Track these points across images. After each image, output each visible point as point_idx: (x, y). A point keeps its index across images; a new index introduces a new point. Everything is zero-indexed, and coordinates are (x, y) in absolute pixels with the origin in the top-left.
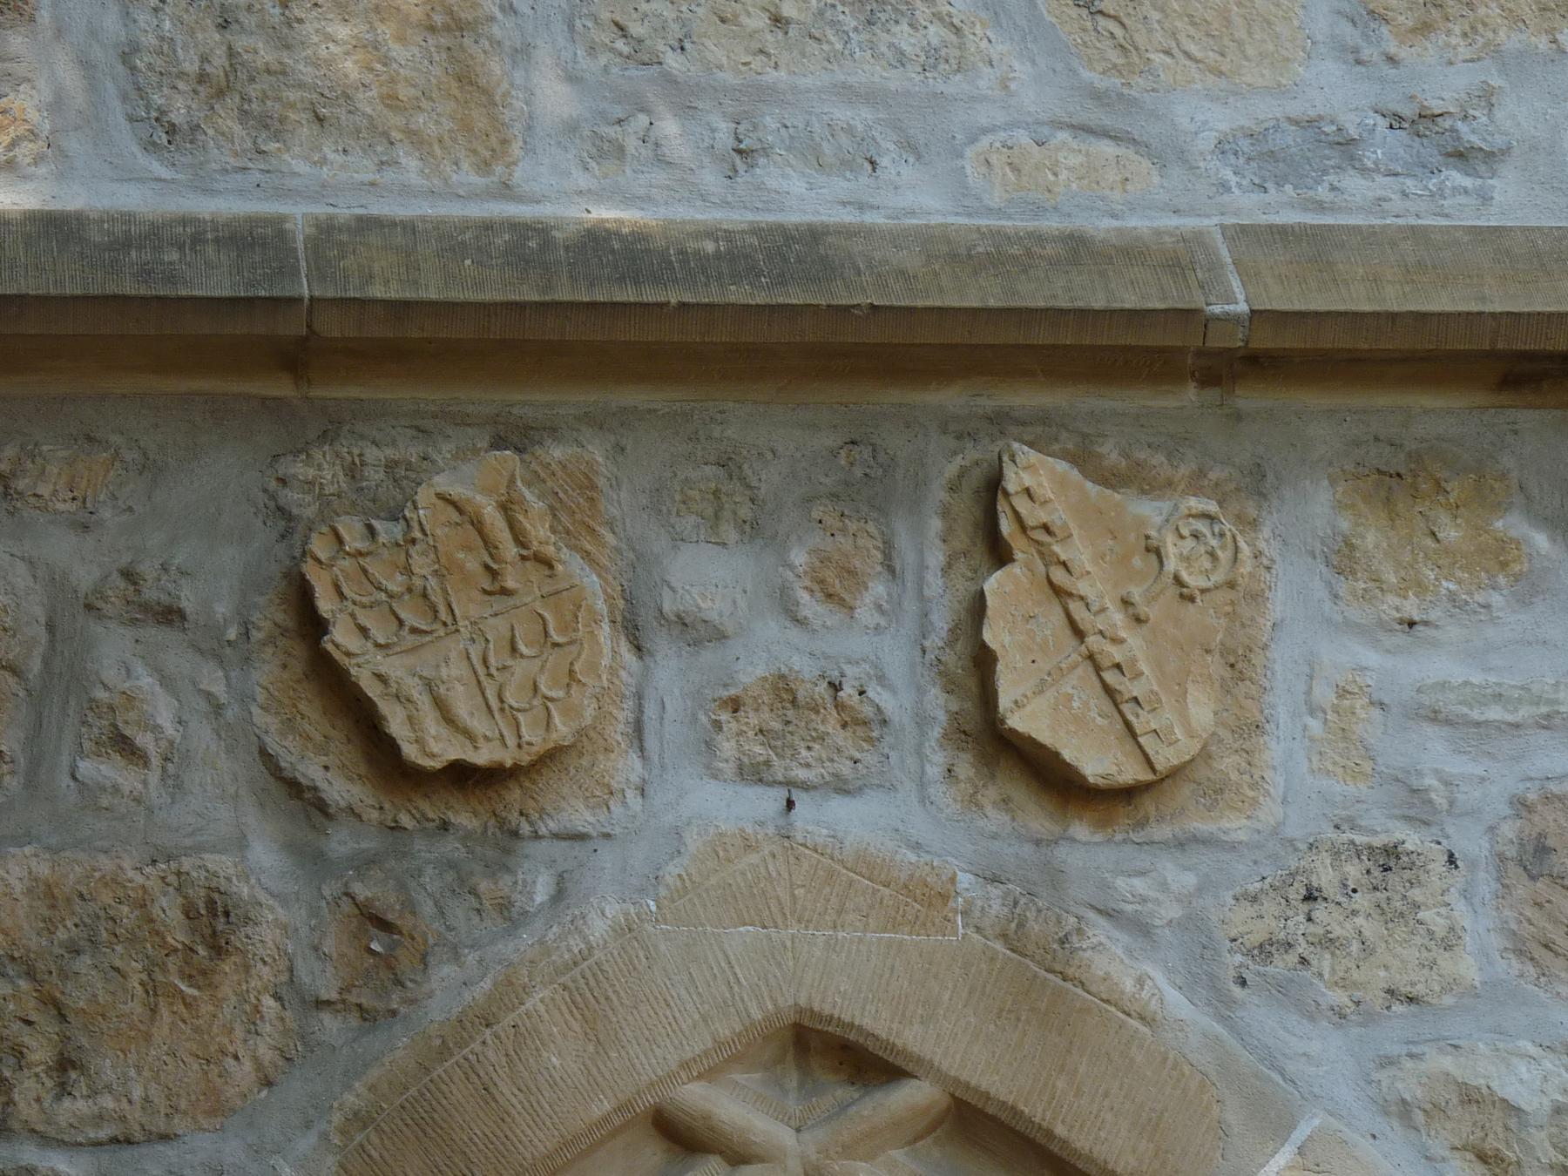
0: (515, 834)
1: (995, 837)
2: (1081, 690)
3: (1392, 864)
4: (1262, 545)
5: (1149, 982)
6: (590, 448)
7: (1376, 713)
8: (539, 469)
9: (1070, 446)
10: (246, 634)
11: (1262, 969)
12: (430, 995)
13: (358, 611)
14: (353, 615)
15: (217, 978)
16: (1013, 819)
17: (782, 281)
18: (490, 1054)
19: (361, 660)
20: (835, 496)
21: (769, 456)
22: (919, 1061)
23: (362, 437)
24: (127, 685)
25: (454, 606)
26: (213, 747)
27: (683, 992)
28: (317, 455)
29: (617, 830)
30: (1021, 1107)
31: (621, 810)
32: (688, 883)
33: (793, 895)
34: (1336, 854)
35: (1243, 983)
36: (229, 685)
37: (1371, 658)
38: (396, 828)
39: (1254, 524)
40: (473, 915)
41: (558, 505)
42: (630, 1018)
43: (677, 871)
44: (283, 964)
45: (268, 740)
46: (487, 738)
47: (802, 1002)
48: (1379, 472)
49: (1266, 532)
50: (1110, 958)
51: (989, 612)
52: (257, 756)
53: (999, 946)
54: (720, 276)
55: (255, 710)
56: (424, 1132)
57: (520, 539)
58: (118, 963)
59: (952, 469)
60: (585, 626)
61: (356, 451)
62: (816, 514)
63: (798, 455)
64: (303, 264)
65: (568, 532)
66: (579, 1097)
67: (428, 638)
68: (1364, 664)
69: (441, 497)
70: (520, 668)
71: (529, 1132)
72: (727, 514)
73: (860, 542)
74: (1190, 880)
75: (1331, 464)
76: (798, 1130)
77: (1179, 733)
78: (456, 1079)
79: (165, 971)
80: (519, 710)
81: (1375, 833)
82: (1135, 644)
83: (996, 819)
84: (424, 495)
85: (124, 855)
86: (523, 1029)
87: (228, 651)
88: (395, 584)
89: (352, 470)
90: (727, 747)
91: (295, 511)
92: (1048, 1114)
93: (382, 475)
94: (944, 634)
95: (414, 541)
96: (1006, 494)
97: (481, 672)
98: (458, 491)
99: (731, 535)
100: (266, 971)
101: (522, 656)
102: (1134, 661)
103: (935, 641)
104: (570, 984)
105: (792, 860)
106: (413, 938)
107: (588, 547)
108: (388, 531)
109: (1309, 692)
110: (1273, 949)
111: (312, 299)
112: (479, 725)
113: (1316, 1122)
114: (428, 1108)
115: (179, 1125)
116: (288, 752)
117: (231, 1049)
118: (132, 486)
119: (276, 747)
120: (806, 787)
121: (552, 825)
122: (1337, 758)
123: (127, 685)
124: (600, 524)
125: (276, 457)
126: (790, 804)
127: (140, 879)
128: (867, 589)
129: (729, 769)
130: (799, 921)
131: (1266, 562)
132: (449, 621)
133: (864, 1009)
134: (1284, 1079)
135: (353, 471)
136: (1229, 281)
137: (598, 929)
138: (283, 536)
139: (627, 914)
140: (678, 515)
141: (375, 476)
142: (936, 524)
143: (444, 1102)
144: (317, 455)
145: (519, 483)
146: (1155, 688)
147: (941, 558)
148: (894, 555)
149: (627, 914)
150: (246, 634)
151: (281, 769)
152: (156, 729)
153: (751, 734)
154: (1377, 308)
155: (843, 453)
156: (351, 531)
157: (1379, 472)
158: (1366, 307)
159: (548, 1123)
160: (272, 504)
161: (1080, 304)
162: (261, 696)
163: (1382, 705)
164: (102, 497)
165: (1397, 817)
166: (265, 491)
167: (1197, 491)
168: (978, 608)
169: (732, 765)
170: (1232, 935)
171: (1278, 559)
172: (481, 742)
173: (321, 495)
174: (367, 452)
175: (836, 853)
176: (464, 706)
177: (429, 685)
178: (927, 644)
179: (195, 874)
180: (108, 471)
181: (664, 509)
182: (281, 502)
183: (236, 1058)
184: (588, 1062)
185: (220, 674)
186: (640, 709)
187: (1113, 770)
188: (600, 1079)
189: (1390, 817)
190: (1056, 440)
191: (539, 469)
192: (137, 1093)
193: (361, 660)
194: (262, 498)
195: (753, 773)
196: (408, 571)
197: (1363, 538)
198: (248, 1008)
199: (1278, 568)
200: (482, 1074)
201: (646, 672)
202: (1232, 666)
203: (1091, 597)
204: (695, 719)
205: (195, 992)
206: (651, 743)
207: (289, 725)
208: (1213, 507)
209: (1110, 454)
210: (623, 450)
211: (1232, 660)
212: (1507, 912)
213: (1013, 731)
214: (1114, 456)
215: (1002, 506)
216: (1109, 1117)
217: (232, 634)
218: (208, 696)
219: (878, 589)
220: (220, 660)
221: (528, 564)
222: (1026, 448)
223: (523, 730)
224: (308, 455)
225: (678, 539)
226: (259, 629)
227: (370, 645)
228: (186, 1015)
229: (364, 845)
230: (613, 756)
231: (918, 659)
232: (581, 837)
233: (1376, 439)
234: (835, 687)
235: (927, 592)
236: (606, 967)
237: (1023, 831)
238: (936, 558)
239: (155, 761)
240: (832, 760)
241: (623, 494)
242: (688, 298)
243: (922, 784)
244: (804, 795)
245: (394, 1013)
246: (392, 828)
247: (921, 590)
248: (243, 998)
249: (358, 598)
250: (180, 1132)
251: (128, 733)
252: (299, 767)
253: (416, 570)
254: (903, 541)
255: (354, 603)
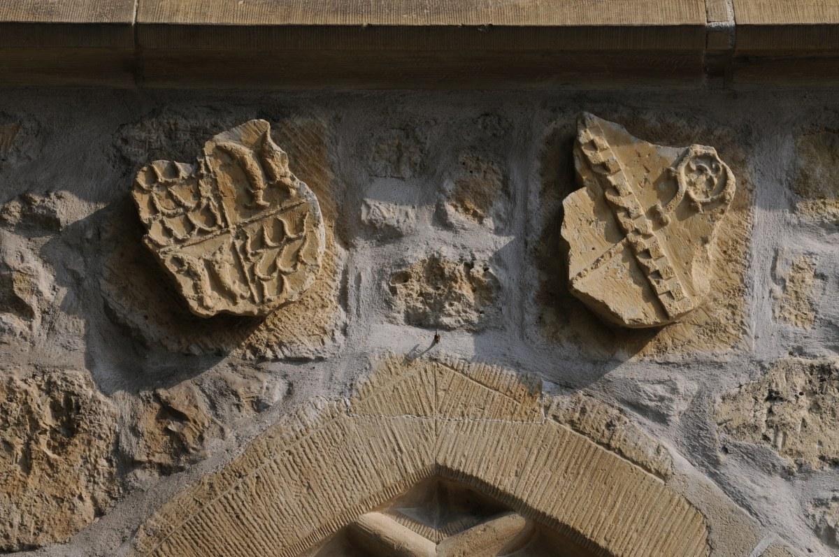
0: (263, 359)
1: (567, 359)
2: (617, 264)
3: (826, 377)
4: (747, 176)
5: (663, 450)
6: (320, 119)
7: (819, 282)
8: (286, 132)
9: (625, 115)
10: (99, 234)
11: (738, 442)
12: (204, 458)
13: (165, 219)
14: (162, 222)
15: (70, 448)
16: (580, 348)
17: (437, 11)
18: (241, 494)
19: (166, 249)
20: (473, 148)
21: (432, 123)
22: (514, 499)
23: (176, 113)
24: (22, 266)
25: (227, 215)
26: (75, 304)
27: (365, 456)
28: (148, 124)
29: (327, 356)
30: (578, 528)
31: (331, 343)
32: (371, 388)
33: (437, 395)
34: (789, 371)
35: (725, 450)
36: (86, 266)
37: (815, 245)
38: (189, 355)
39: (743, 163)
40: (234, 408)
41: (298, 155)
42: (330, 471)
43: (365, 380)
44: (112, 439)
45: (109, 300)
46: (242, 297)
47: (440, 462)
48: (827, 129)
49: (750, 168)
50: (641, 434)
51: (566, 218)
52: (102, 310)
53: (568, 428)
54: (399, 8)
55: (102, 281)
56: (197, 543)
57: (268, 173)
58: (8, 438)
59: (548, 131)
60: (307, 227)
61: (172, 121)
62: (461, 159)
63: (451, 122)
64: (718, 159)
65: (304, 171)
66: (296, 521)
67: (210, 236)
68: (811, 251)
69: (219, 148)
70: (266, 255)
71: (263, 543)
72: (404, 159)
73: (489, 176)
74: (694, 387)
75: (794, 125)
76: (438, 543)
77: (685, 293)
78: (218, 511)
79: (37, 442)
80: (264, 280)
81: (815, 357)
82: (659, 236)
83: (568, 348)
84: (209, 148)
85: (15, 371)
86: (262, 479)
87: (87, 245)
88: (190, 203)
89: (170, 134)
90: (400, 304)
91: (133, 159)
92: (595, 533)
93: (188, 137)
94: (539, 233)
95: (202, 176)
96: (579, 144)
97: (239, 256)
98: (231, 144)
99: (406, 171)
100: (102, 444)
101: (268, 247)
102: (657, 249)
103: (533, 237)
104: (294, 451)
105: (437, 374)
106: (195, 422)
107: (316, 180)
108: (184, 170)
109: (774, 268)
110: (746, 431)
111: (137, 23)
112: (237, 288)
113: (771, 540)
114: (200, 528)
115: (43, 540)
116: (122, 307)
117: (78, 492)
118: (29, 144)
119: (114, 304)
120: (448, 328)
121: (287, 353)
122: (792, 310)
123: (22, 266)
124: (324, 166)
125: (122, 126)
126: (437, 339)
127: (24, 386)
128: (491, 205)
129: (401, 317)
130: (440, 412)
131: (749, 187)
132: (223, 225)
133: (479, 466)
134: (751, 513)
135: (171, 134)
136: (725, 9)
137: (311, 416)
138: (124, 175)
139: (331, 407)
140: (374, 160)
141: (184, 137)
142: (537, 164)
143: (210, 524)
144: (148, 124)
145: (269, 139)
146: (671, 264)
147: (539, 186)
148: (510, 183)
149: (331, 407)
150: (99, 234)
151: (117, 318)
152: (39, 293)
153: (415, 296)
154: (819, 22)
155: (480, 121)
156: (160, 167)
157: (827, 129)
158: (812, 21)
159: (276, 537)
160: (118, 154)
161: (625, 23)
162: (106, 274)
163: (822, 277)
164: (10, 150)
165: (830, 348)
166: (114, 146)
167: (705, 141)
168: (557, 217)
169: (402, 315)
170: (719, 421)
171: (757, 184)
172: (240, 300)
173: (149, 149)
174: (179, 121)
175: (466, 369)
176: (229, 276)
177: (209, 265)
178: (529, 239)
179: (59, 383)
180: (15, 134)
181: (365, 156)
182: (124, 153)
183: (80, 498)
184: (303, 500)
185: (81, 259)
186: (345, 281)
187: (642, 316)
188: (309, 510)
189: (826, 347)
190: (616, 111)
191: (286, 132)
192: (17, 520)
193: (166, 249)
194: (112, 151)
195: (416, 320)
196: (197, 195)
197: (814, 171)
198: (89, 466)
199: (757, 191)
200: (235, 507)
201: (350, 259)
202: (725, 252)
203: (631, 208)
204: (379, 286)
205: (56, 456)
206: (352, 302)
207: (124, 290)
208: (712, 151)
209: (651, 120)
210: (340, 119)
211: (725, 249)
212: (306, 274)
213: (577, 291)
214: (653, 121)
215: (576, 152)
216: (635, 535)
217: (89, 235)
218: (74, 273)
219: (499, 205)
220: (81, 250)
221: (274, 190)
222: (592, 115)
223: (266, 292)
224: (142, 124)
225: (373, 175)
226: (106, 232)
227: (172, 240)
228: (49, 471)
229: (168, 365)
230: (327, 310)
231: (522, 249)
232: (305, 360)
233: (826, 108)
234: (469, 266)
235: (529, 207)
236: (317, 440)
237: (586, 356)
238: (536, 186)
239: (37, 314)
240: (466, 312)
241: (340, 148)
242: (375, 22)
243: (522, 327)
244: (448, 334)
245: (182, 469)
246: (187, 355)
247: (525, 206)
248: (86, 461)
249: (166, 211)
250: (42, 544)
251: (20, 295)
252: (129, 317)
253: (203, 193)
254: (516, 177)
255: (163, 214)
